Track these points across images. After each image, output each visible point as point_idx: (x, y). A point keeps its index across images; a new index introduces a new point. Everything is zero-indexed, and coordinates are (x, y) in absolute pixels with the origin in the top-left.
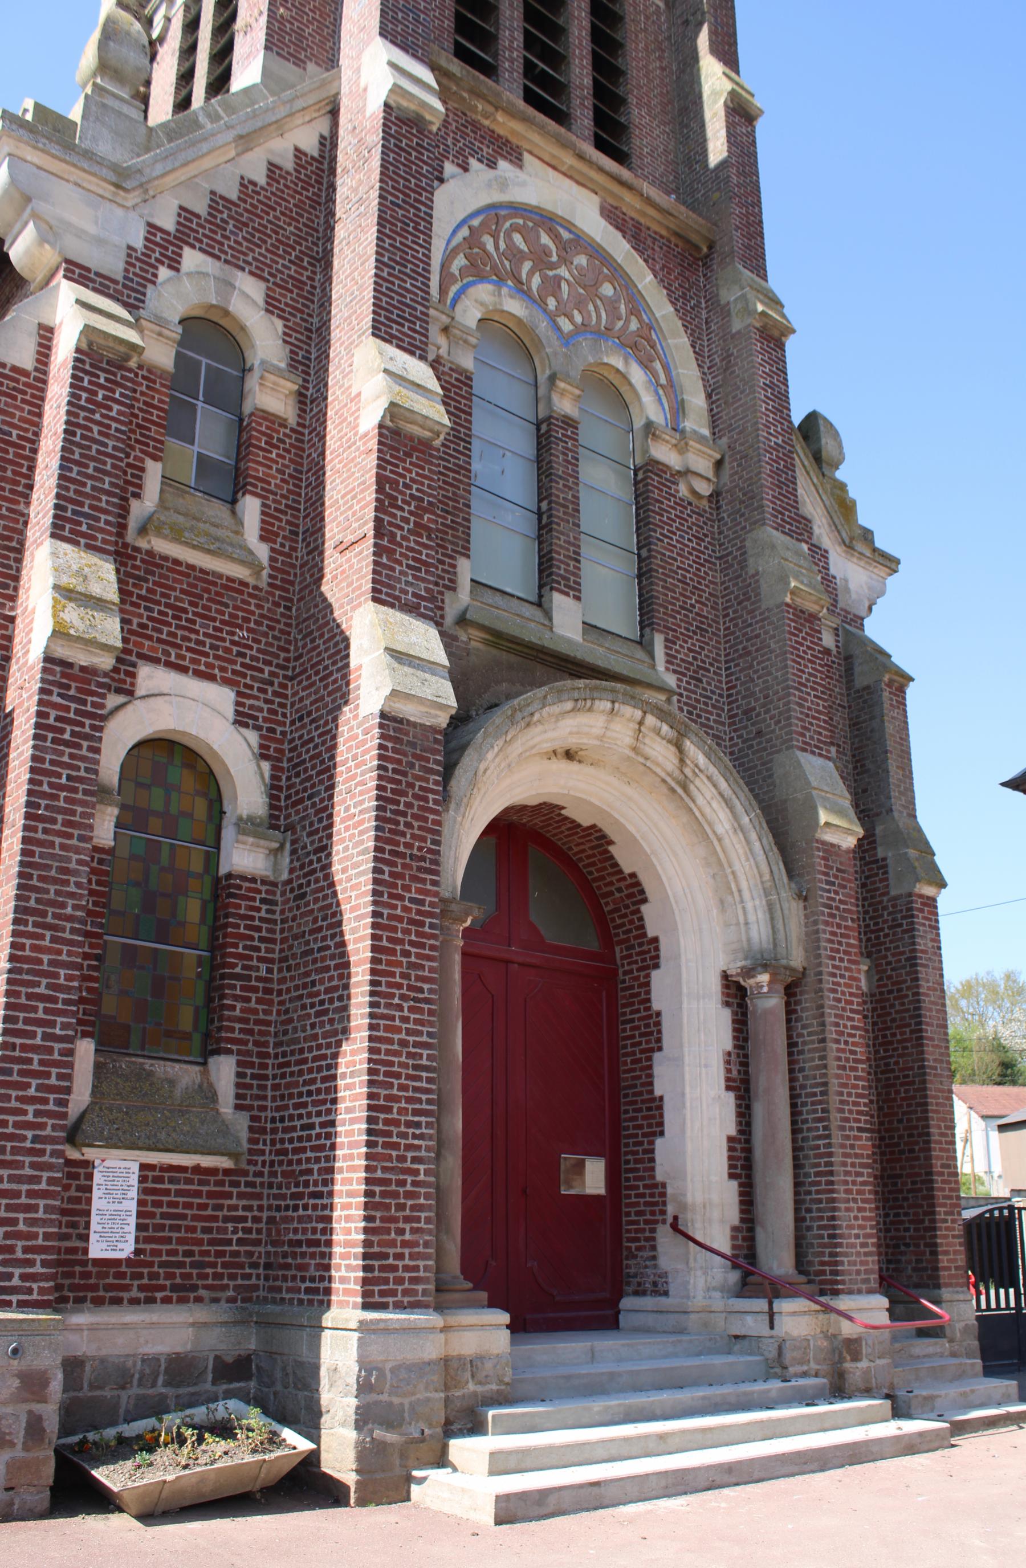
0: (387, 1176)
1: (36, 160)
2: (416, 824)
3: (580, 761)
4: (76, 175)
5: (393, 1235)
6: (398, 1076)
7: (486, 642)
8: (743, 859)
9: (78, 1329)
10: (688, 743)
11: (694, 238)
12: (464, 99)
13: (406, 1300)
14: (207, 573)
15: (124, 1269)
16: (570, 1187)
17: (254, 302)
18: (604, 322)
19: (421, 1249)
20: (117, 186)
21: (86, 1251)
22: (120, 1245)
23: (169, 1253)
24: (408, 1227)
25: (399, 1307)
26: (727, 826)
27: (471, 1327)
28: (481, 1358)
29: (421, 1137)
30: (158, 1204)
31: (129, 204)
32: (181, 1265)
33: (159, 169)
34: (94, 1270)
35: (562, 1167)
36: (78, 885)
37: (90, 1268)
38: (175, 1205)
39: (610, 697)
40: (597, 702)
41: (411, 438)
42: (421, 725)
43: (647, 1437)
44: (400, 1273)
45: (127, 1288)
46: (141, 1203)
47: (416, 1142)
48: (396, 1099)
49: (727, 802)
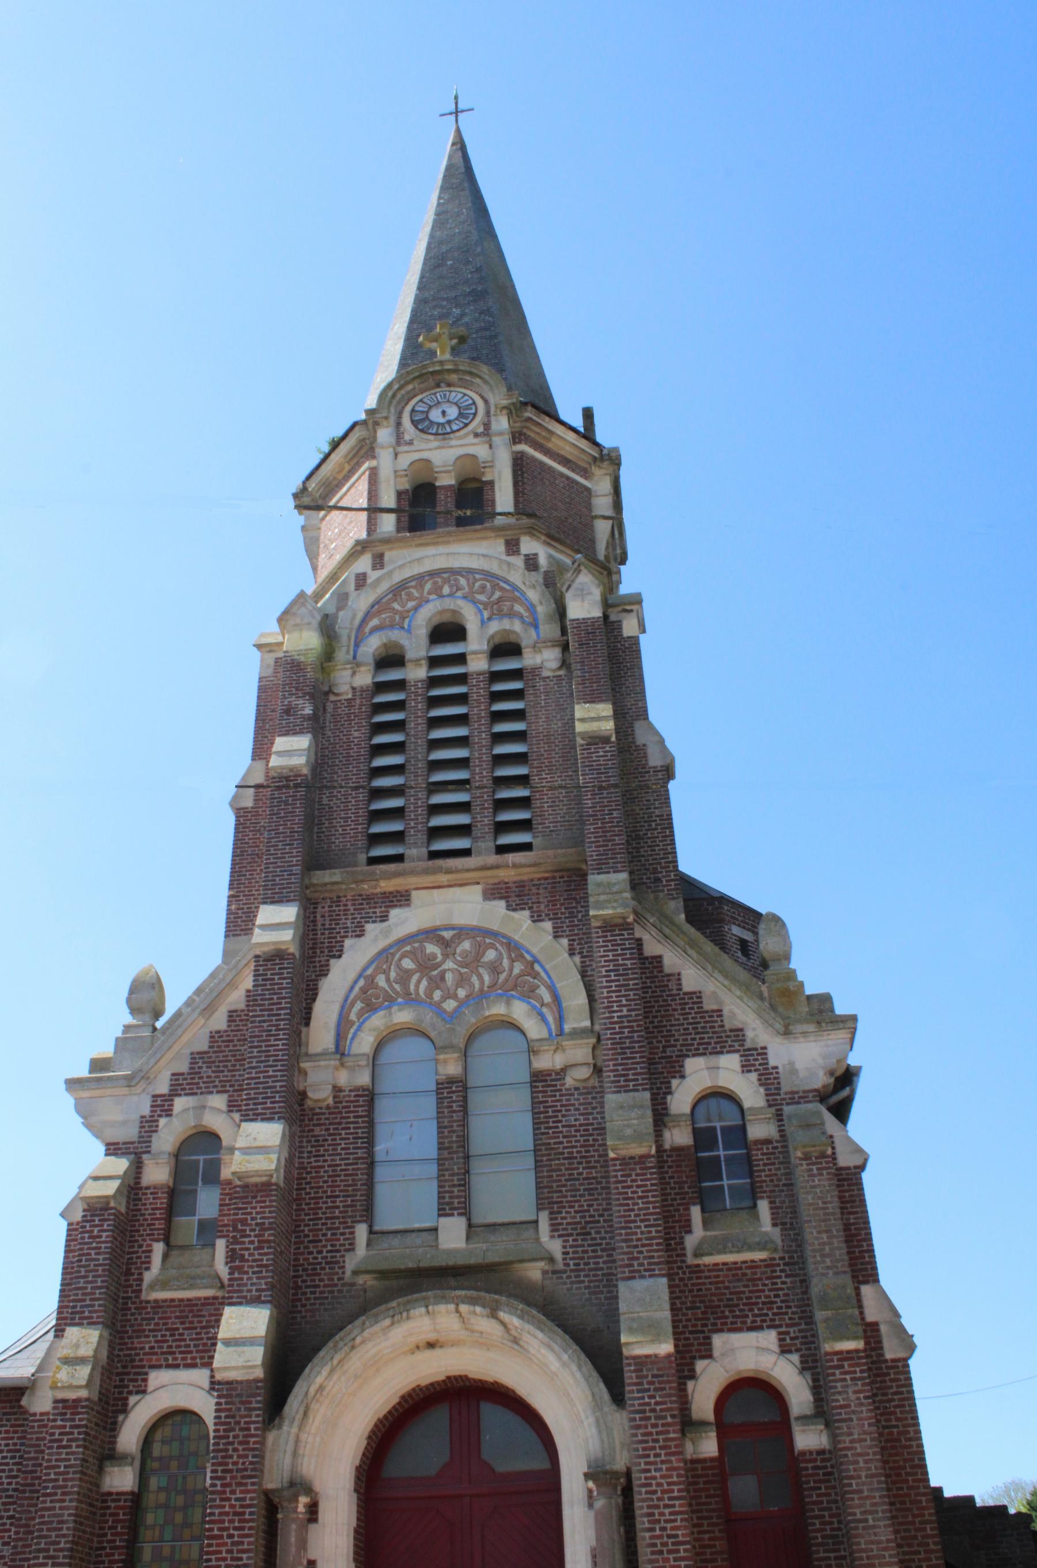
2: (240, 1448)
3: (441, 1347)
4: (109, 1092)
7: (376, 1279)
17: (219, 1110)
18: (487, 983)
20: (129, 1086)
31: (139, 1091)
33: (152, 1061)
36: (68, 1529)
40: (412, 1311)
41: (256, 1185)
49: (549, 1347)
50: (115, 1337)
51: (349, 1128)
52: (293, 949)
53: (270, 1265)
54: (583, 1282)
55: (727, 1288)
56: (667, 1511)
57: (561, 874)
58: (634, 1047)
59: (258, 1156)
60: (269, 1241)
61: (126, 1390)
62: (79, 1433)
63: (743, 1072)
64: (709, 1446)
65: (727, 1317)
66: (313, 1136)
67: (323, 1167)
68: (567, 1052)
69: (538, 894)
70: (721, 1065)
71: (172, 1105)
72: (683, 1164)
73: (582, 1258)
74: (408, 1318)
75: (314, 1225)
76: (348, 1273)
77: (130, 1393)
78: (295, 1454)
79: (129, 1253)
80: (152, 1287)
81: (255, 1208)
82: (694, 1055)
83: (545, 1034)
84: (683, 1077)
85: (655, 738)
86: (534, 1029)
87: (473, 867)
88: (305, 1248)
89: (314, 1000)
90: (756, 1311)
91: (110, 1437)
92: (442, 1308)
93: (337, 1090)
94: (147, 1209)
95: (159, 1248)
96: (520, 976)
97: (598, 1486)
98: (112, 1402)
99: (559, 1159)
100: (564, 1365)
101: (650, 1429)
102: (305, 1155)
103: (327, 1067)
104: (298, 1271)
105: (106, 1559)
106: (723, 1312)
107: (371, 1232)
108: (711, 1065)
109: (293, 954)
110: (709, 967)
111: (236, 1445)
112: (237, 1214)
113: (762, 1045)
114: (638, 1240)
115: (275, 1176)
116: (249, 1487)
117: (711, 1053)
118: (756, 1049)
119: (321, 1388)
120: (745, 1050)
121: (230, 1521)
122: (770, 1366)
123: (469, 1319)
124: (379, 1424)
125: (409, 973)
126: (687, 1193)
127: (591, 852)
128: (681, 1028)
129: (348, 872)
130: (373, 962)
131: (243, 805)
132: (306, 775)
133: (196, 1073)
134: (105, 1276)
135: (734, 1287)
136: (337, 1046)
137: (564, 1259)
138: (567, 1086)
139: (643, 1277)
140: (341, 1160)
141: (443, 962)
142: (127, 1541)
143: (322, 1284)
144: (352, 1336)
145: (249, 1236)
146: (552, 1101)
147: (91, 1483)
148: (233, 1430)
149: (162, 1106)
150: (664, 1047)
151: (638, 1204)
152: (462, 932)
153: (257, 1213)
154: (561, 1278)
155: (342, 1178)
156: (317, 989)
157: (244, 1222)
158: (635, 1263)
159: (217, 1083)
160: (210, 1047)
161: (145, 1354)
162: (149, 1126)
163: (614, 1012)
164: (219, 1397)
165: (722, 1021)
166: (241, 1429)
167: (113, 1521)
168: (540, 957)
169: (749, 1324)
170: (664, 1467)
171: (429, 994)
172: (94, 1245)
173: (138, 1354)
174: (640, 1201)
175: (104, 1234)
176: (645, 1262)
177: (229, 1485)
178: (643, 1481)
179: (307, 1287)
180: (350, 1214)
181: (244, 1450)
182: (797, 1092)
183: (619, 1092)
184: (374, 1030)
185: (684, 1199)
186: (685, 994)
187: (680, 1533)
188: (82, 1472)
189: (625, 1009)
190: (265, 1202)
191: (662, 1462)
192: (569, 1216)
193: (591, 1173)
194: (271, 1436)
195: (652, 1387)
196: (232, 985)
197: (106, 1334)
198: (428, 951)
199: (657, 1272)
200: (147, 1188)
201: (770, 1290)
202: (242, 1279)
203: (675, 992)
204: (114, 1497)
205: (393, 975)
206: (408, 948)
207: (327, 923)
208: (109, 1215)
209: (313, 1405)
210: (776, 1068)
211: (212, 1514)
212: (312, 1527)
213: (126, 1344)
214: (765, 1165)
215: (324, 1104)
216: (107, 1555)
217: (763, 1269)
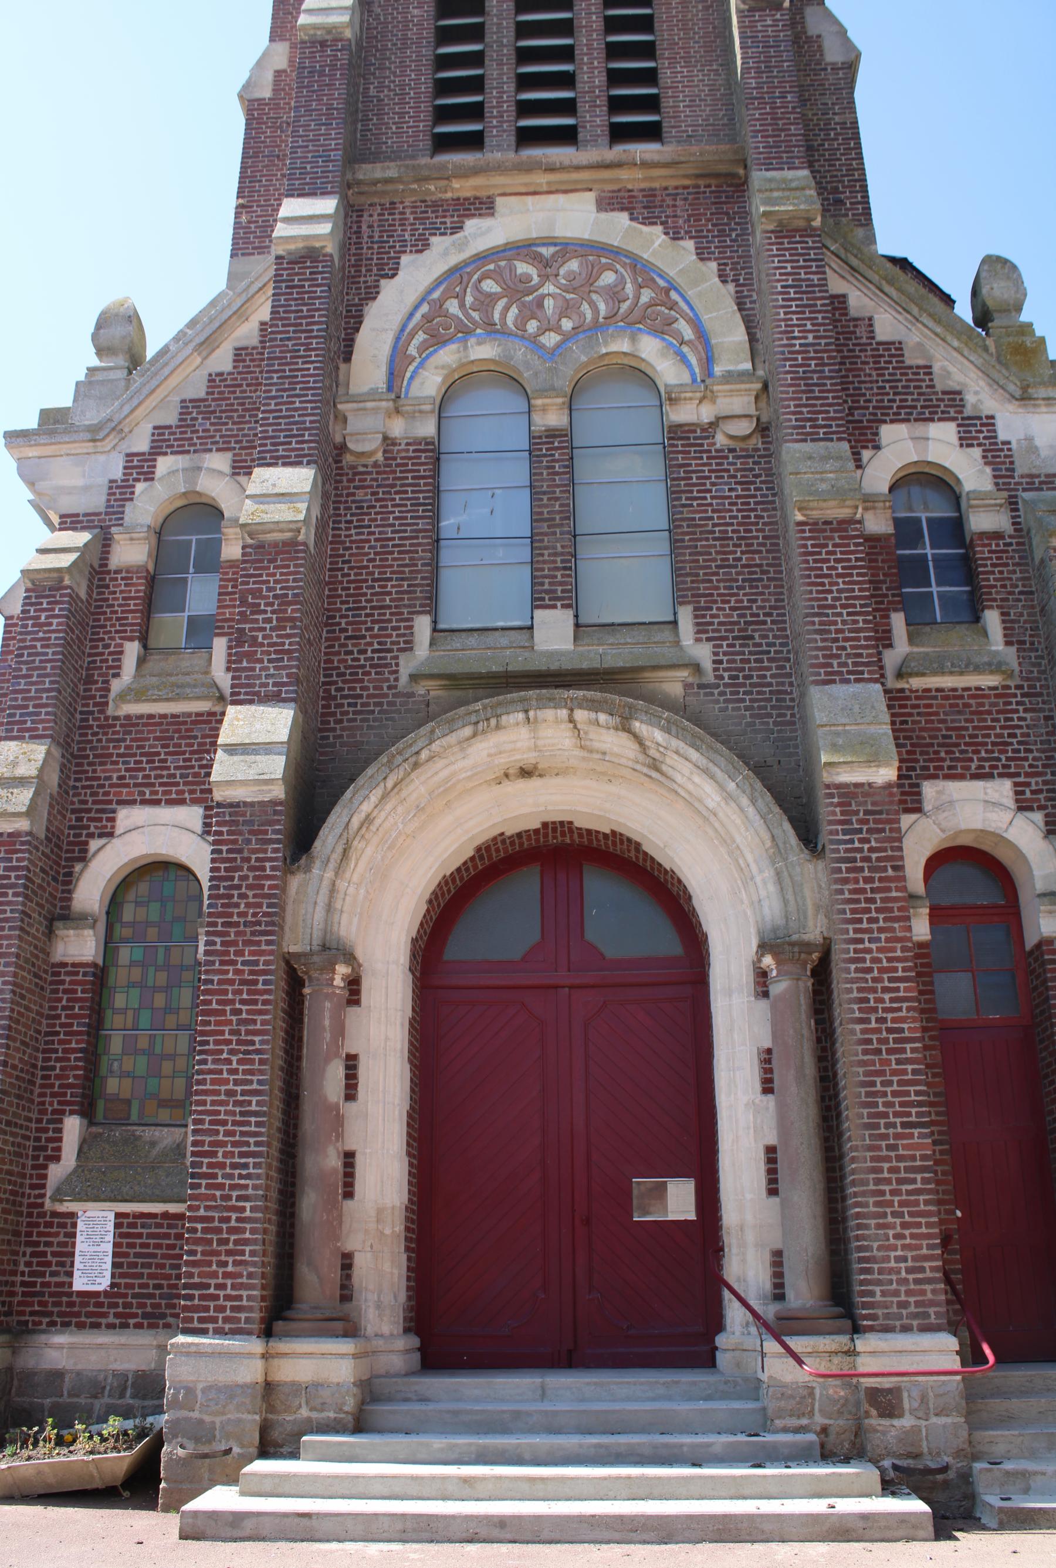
0: (210, 1214)
1: (36, 454)
3: (540, 776)
4: (64, 448)
5: (214, 1267)
6: (224, 1123)
7: (444, 687)
8: (743, 830)
9: (61, 1347)
10: (637, 724)
11: (722, 168)
12: (415, 190)
13: (227, 1326)
14: (178, 716)
15: (102, 1299)
16: (646, 1213)
17: (220, 472)
19: (244, 1280)
20: (94, 441)
21: (71, 1285)
22: (98, 1280)
23: (141, 1286)
24: (230, 1259)
25: (219, 1332)
26: (718, 798)
27: (310, 1355)
28: (317, 1385)
29: (248, 1176)
30: (172, 1247)
32: (151, 1296)
33: (127, 409)
34: (78, 1300)
35: (635, 1192)
37: (74, 1298)
38: (147, 1246)
39: (520, 706)
40: (504, 717)
41: (275, 544)
42: (259, 802)
43: (444, 1478)
44: (221, 1302)
45: (104, 1315)
46: (116, 1245)
47: (242, 1182)
48: (222, 1144)
49: (706, 771)
50: (69, 761)
51: (406, 492)
52: (330, 248)
53: (295, 651)
54: (743, 700)
55: (944, 721)
56: (886, 997)
57: (708, 182)
58: (825, 385)
59: (278, 506)
60: (292, 619)
61: (85, 832)
62: (18, 877)
63: (961, 445)
64: (921, 928)
65: (943, 760)
66: (353, 502)
67: (369, 541)
68: (719, 401)
69: (674, 206)
70: (931, 435)
71: (154, 467)
72: (880, 558)
73: (743, 669)
74: (498, 727)
75: (353, 616)
76: (404, 679)
77: (91, 836)
78: (329, 908)
79: (90, 655)
80: (122, 697)
81: (274, 575)
82: (892, 421)
83: (686, 378)
84: (877, 448)
85: (835, 28)
86: (668, 371)
87: (585, 163)
88: (340, 646)
89: (357, 330)
90: (983, 754)
91: (63, 891)
92: (549, 714)
93: (388, 441)
94: (117, 599)
95: (132, 650)
96: (650, 305)
97: (779, 963)
98: (65, 847)
99: (707, 539)
100: (729, 797)
101: (861, 885)
102: (343, 526)
103: (375, 410)
104: (331, 676)
105: (60, 1048)
106: (937, 752)
107: (435, 630)
108: (917, 434)
109: (331, 255)
110: (915, 311)
111: (243, 890)
112: (248, 583)
113: (990, 413)
114: (837, 631)
115: (303, 531)
116: (264, 947)
117: (916, 420)
118: (979, 418)
119: (368, 820)
120: (963, 419)
121: (235, 992)
122: (1005, 826)
123: (586, 733)
124: (446, 882)
125: (493, 298)
126: (886, 596)
127: (754, 145)
128: (875, 385)
129: (407, 166)
130: (441, 283)
131: (258, 95)
132: (349, 40)
133: (188, 426)
134: (55, 675)
135: (953, 721)
136: (390, 389)
137: (715, 670)
138: (718, 446)
139: (847, 681)
140: (393, 532)
141: (541, 285)
142: (89, 1025)
143: (365, 693)
144: (415, 749)
145: (265, 612)
146: (697, 465)
147: (36, 947)
148: (241, 869)
149: (140, 467)
150: (850, 409)
151: (837, 584)
152: (567, 248)
153: (276, 582)
154: (712, 694)
155: (396, 555)
156: (362, 316)
157: (257, 593)
158: (835, 663)
159: (218, 439)
160: (208, 393)
161: (111, 786)
162: (120, 493)
163: (795, 338)
164: (215, 843)
165: (931, 380)
166: (251, 869)
167: (69, 1000)
168: (680, 281)
169: (973, 770)
170: (883, 936)
171: (521, 323)
172: (41, 635)
173: (103, 786)
174: (840, 580)
175: (55, 621)
176: (850, 661)
177: (234, 943)
178: (852, 955)
179: (343, 697)
180: (406, 602)
181: (255, 896)
182: (1039, 476)
183: (805, 441)
184: (443, 367)
185: (882, 603)
186: (879, 344)
187: (905, 1026)
188: (22, 929)
189: (810, 336)
190: (288, 566)
191: (881, 930)
192: (720, 613)
193: (754, 559)
194: (295, 882)
195: (865, 827)
196: (240, 314)
197: (57, 753)
198: (519, 271)
199: (866, 676)
200: (116, 572)
201: (1002, 727)
202: (253, 669)
203: (864, 340)
204: (69, 969)
205: (469, 299)
206: (492, 267)
207: (376, 235)
208: (62, 596)
209: (355, 843)
210: (1009, 443)
211: (207, 982)
212: (352, 1010)
213: (87, 772)
214: (993, 565)
215: (370, 461)
216: (61, 1042)
217: (993, 700)
